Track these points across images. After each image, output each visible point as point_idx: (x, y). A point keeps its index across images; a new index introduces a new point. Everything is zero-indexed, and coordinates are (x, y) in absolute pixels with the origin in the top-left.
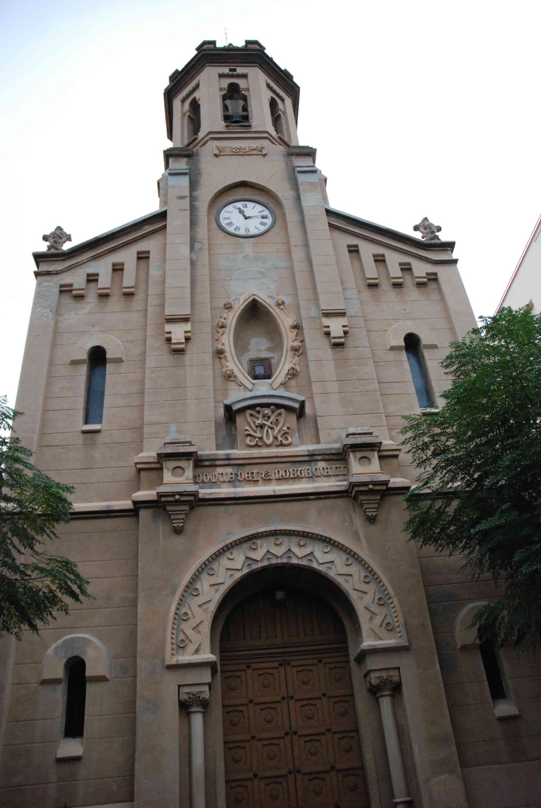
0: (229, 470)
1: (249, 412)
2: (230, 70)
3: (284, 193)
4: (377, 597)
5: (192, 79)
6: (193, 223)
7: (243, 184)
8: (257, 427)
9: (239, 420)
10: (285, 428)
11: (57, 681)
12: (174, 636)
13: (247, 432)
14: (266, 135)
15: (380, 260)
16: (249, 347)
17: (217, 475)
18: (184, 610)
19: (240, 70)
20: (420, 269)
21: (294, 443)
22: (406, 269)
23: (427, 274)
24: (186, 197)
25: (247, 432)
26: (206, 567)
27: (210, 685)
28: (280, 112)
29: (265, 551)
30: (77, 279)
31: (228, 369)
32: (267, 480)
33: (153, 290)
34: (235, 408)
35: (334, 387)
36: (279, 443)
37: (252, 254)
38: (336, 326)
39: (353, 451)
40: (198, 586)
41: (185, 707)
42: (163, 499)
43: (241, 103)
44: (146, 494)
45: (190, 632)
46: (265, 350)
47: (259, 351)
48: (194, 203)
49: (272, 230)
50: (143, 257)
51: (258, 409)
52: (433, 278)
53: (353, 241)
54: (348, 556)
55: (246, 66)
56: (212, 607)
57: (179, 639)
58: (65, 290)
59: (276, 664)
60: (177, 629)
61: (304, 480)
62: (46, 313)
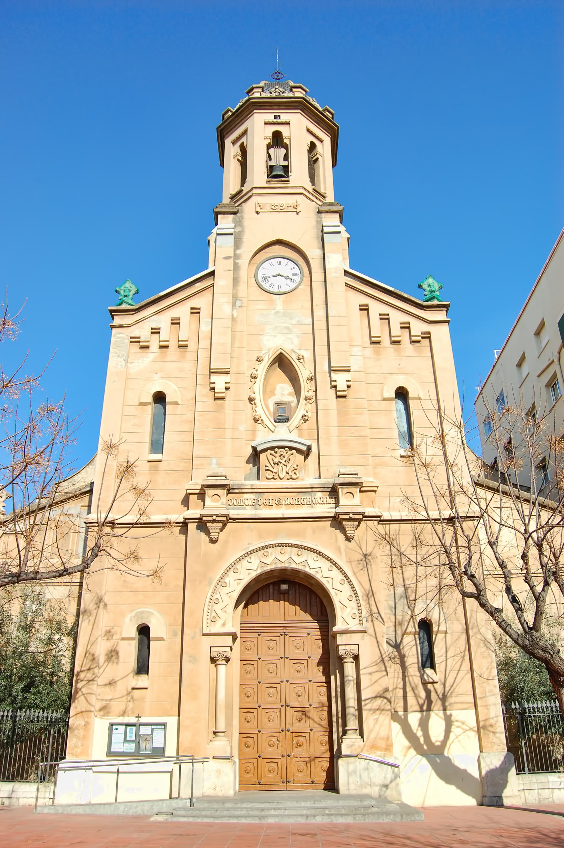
0: (252, 496)
2: (275, 117)
5: (242, 122)
6: (236, 282)
8: (274, 464)
9: (263, 456)
10: (295, 466)
11: (133, 639)
12: (209, 614)
13: (267, 468)
14: (301, 191)
15: (385, 318)
16: (276, 392)
17: (244, 500)
18: (216, 596)
19: (284, 117)
21: (300, 477)
22: (406, 327)
23: (422, 333)
24: (230, 257)
25: (267, 468)
28: (318, 156)
29: (273, 557)
31: (257, 414)
32: (279, 504)
34: (259, 449)
35: (334, 432)
36: (290, 477)
37: (282, 311)
38: (341, 380)
39: (341, 488)
40: (227, 580)
42: (204, 518)
43: (283, 151)
44: (194, 512)
45: (219, 612)
46: (288, 395)
47: (283, 395)
48: (237, 261)
49: (300, 287)
50: (195, 311)
51: (276, 450)
53: (365, 300)
54: (332, 564)
57: (212, 616)
59: (279, 634)
61: (306, 505)
62: (120, 362)
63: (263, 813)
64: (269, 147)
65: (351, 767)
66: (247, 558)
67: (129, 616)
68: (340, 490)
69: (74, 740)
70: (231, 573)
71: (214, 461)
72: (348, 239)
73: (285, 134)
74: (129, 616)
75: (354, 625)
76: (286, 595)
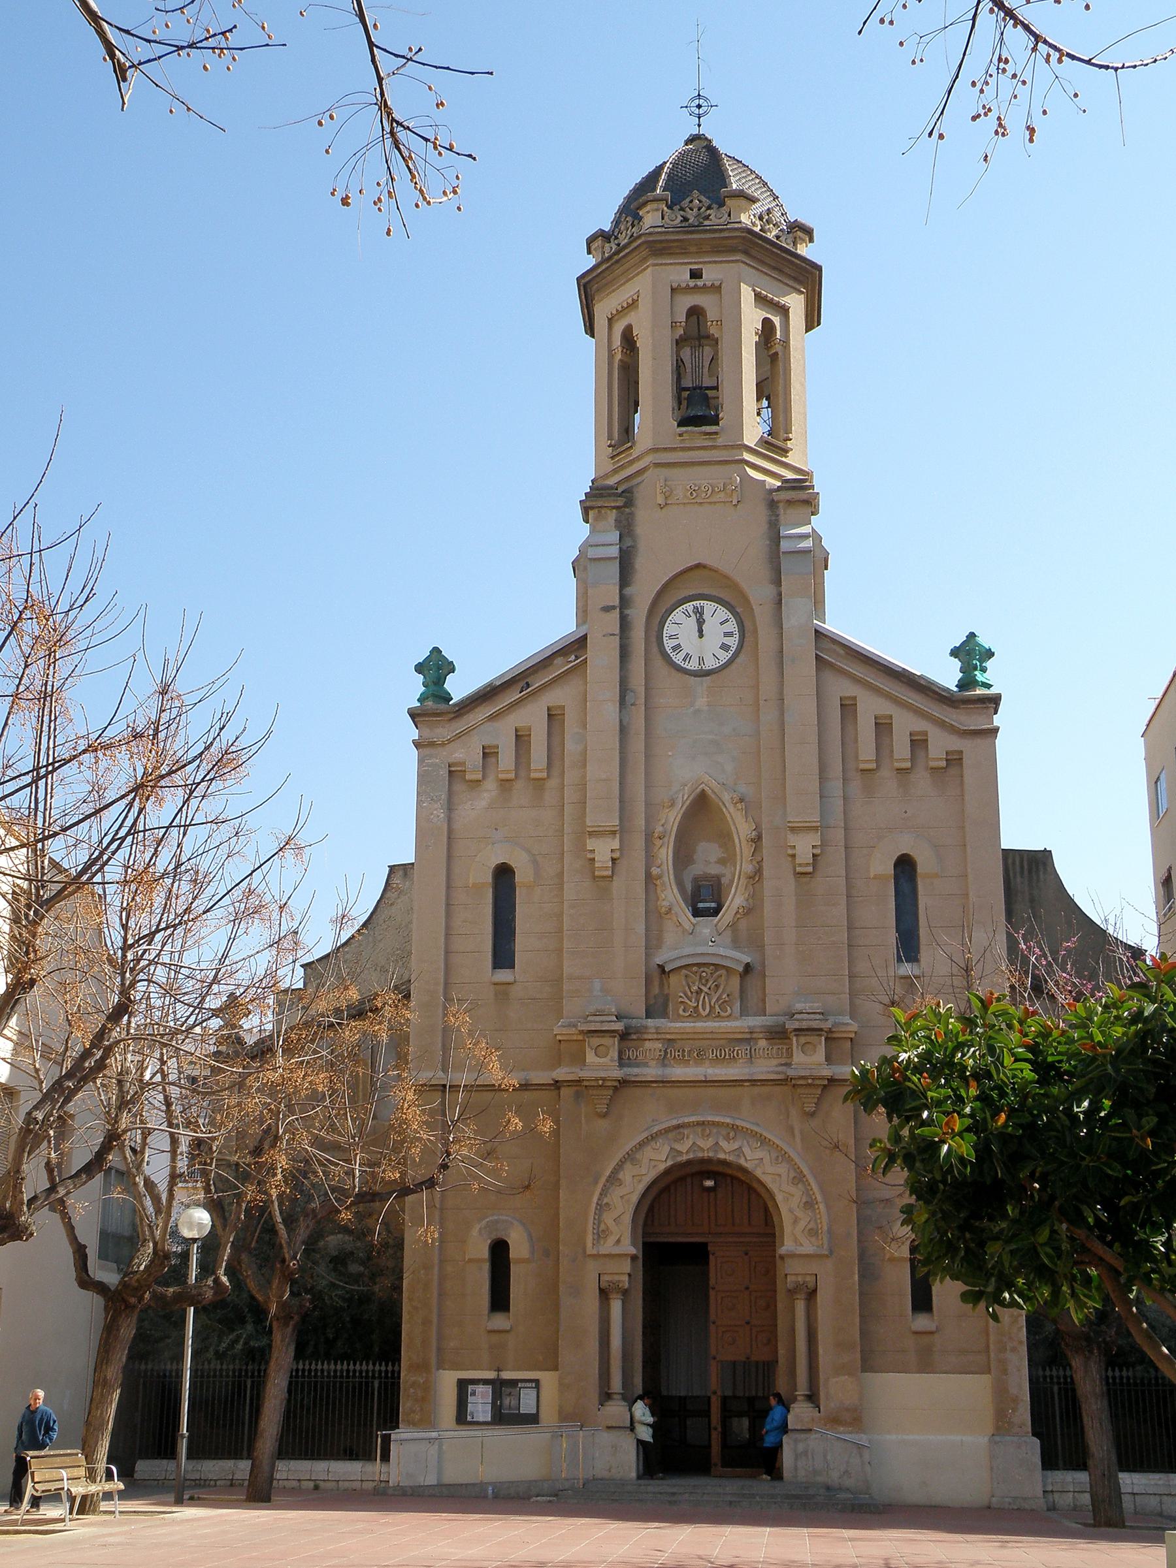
1: (684, 971)
3: (759, 593)
4: (804, 1200)
6: (625, 653)
7: (698, 566)
15: (883, 727)
20: (940, 744)
22: (918, 743)
24: (614, 608)
26: (630, 1157)
27: (629, 1275)
30: (468, 754)
33: (571, 776)
40: (621, 1176)
41: (604, 1294)
46: (638, 1440)
47: (707, 862)
50: (554, 717)
52: (954, 760)
55: (721, 262)
56: (635, 1198)
58: (454, 773)
60: (599, 1221)
63: (674, 1499)
64: (679, 343)
65: (801, 1447)
66: (653, 1143)
67: (478, 1227)
68: (795, 1039)
69: (409, 1404)
70: (628, 1166)
71: (597, 985)
72: (826, 568)
73: (711, 315)
74: (478, 1227)
75: (808, 1248)
76: (712, 1194)
